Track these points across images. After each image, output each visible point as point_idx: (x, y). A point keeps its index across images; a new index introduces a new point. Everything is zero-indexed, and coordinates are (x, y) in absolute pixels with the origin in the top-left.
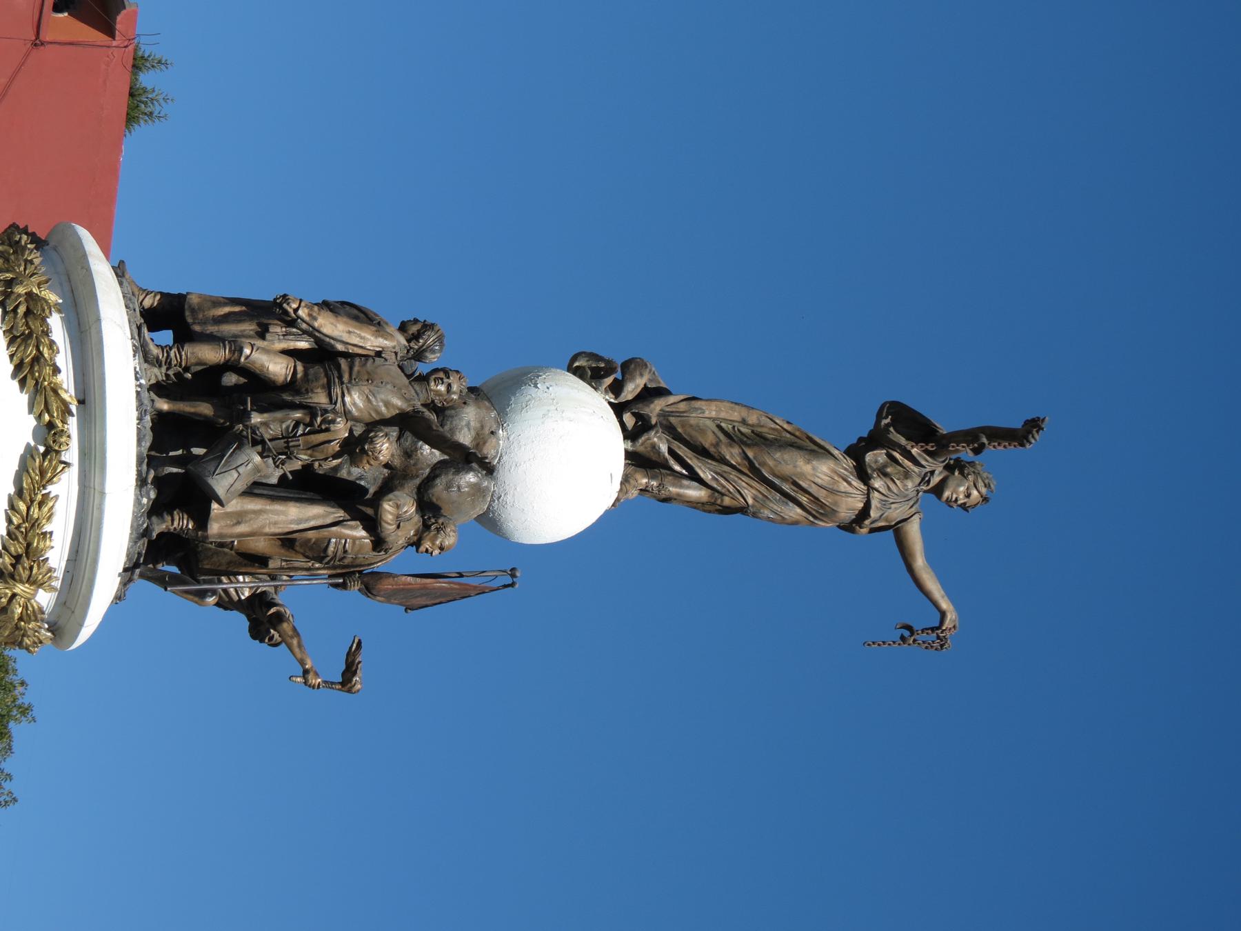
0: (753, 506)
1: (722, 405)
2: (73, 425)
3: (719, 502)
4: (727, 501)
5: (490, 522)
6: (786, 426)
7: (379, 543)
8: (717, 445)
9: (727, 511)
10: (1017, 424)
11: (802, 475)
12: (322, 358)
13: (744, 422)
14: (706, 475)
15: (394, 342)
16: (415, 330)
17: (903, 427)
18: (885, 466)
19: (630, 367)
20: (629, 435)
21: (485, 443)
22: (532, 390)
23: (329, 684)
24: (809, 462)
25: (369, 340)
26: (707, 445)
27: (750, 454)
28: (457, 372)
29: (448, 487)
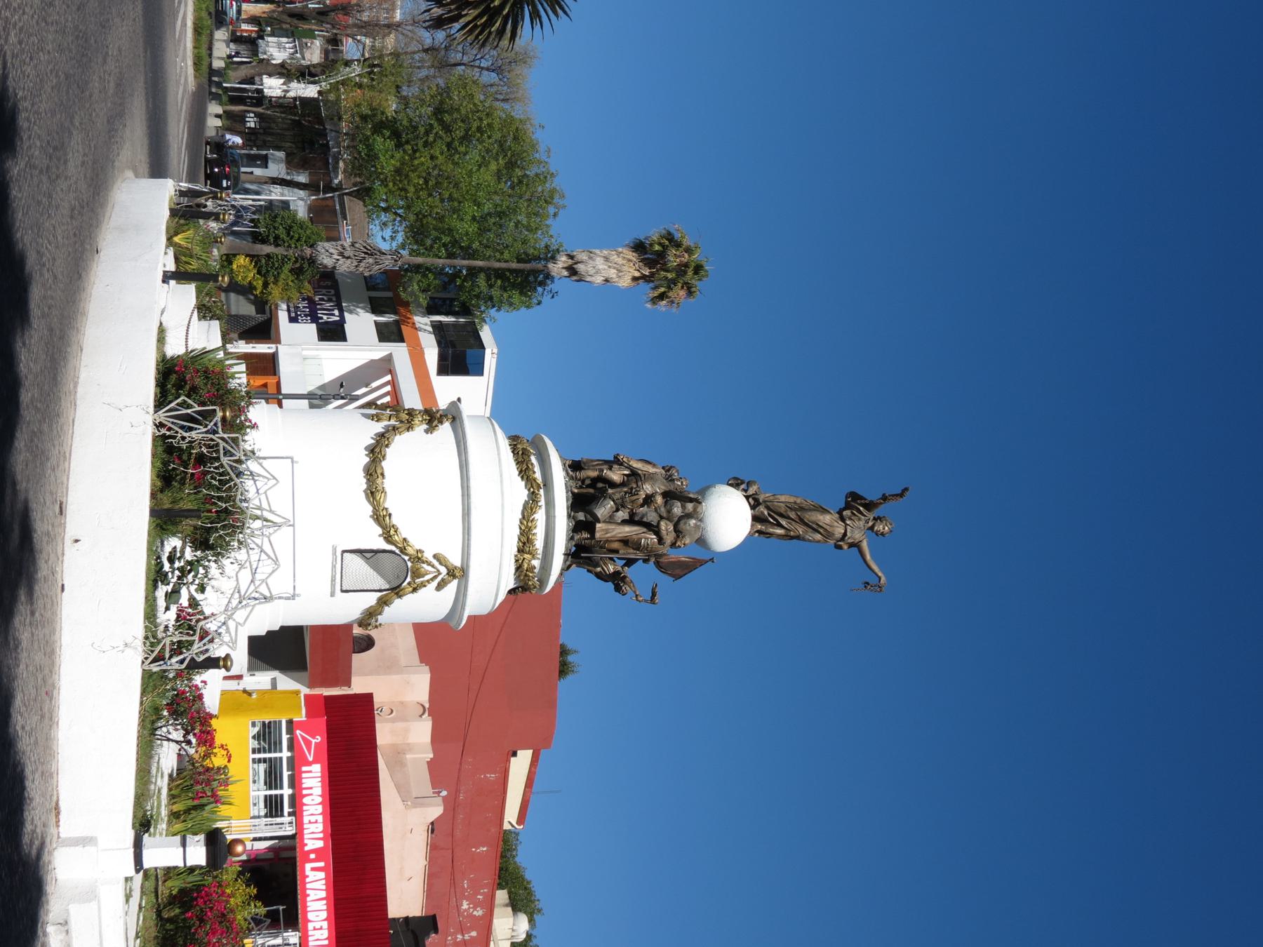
2: (542, 492)
5: (702, 542)
7: (661, 541)
9: (792, 538)
12: (634, 474)
14: (783, 522)
15: (660, 471)
16: (667, 469)
19: (749, 484)
20: (753, 507)
23: (646, 601)
25: (651, 470)
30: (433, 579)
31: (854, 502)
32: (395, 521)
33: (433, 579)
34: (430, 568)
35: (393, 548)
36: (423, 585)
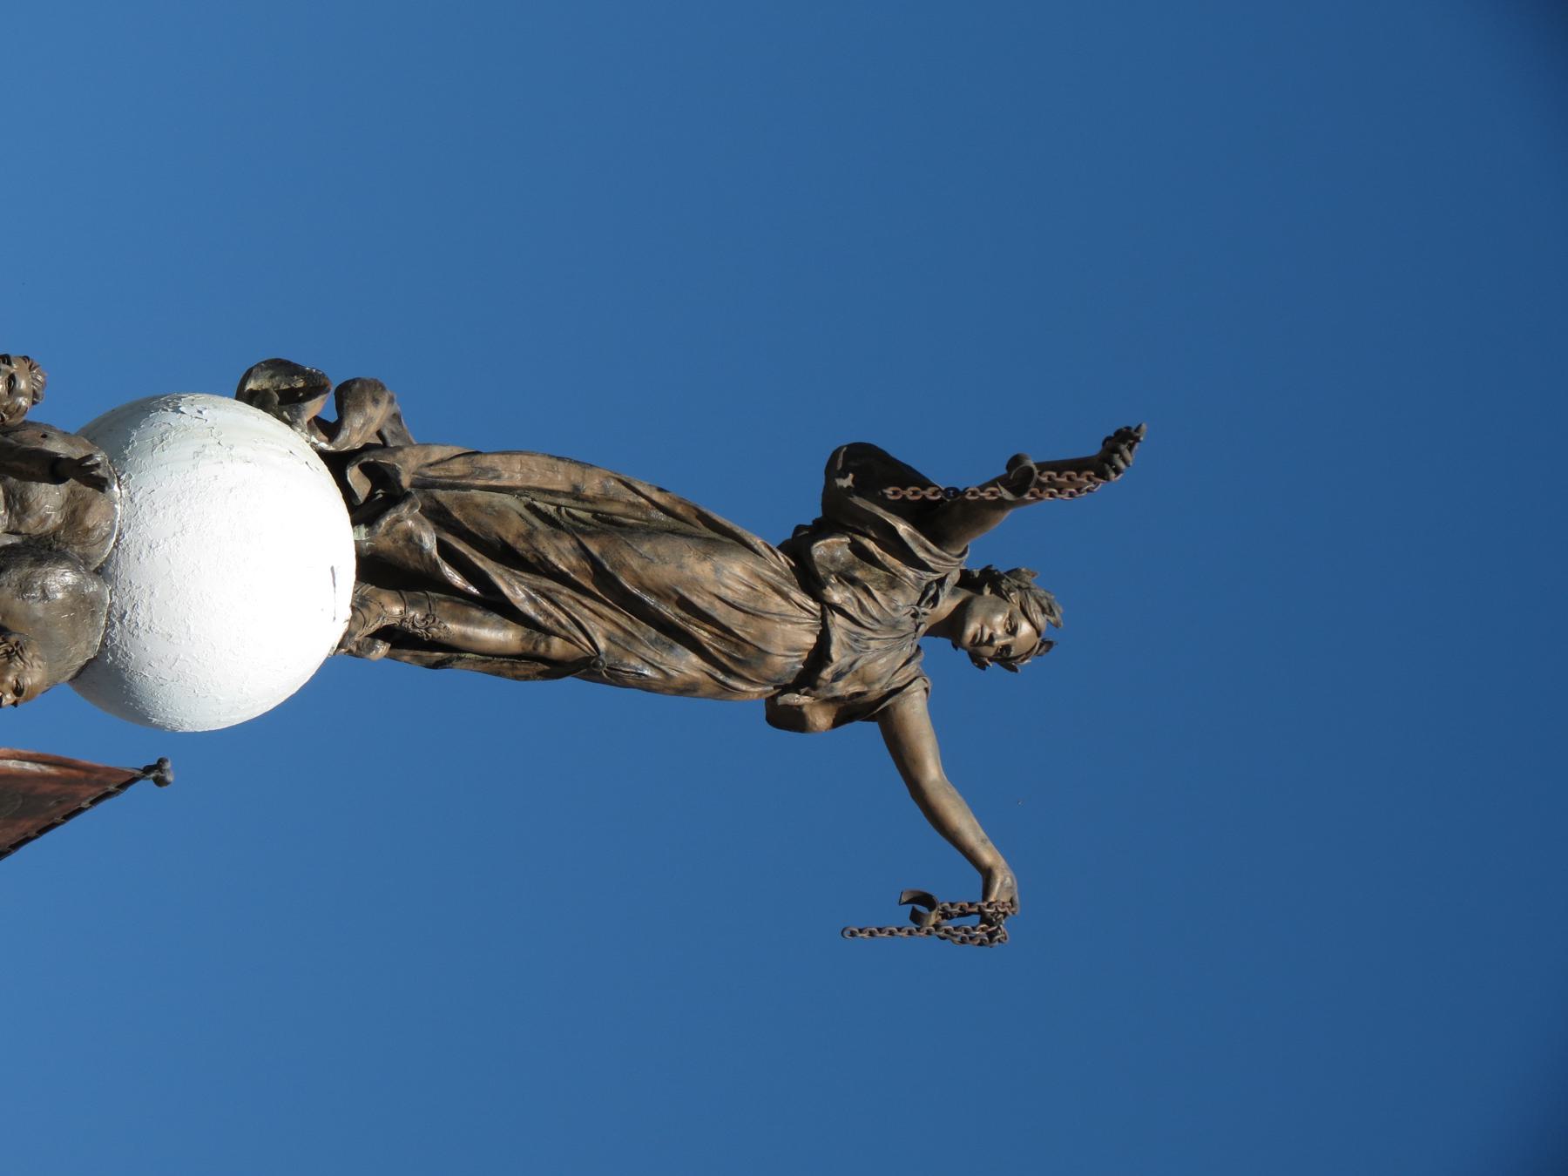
0: (608, 653)
1: (532, 462)
3: (542, 648)
4: (557, 647)
5: (106, 679)
6: (656, 496)
8: (529, 536)
9: (557, 668)
10: (1093, 449)
11: (694, 582)
13: (576, 494)
14: (516, 590)
17: (871, 499)
18: (852, 567)
19: (347, 396)
20: (362, 513)
21: (87, 507)
22: (171, 417)
24: (706, 557)
26: (510, 539)
27: (594, 549)
28: (26, 358)
29: (24, 588)
31: (871, 499)
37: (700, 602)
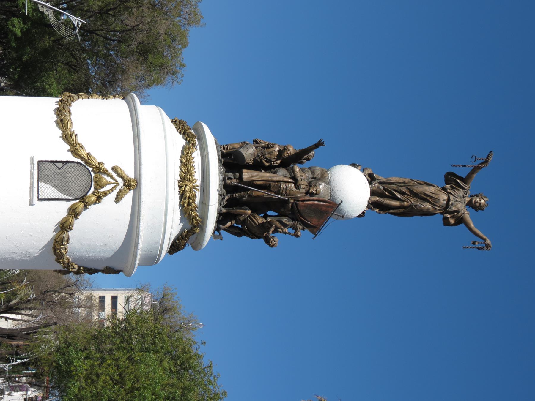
7: (297, 187)
14: (398, 196)
17: (452, 180)
20: (370, 183)
30: (112, 190)
31: (452, 180)
32: (80, 140)
33: (112, 190)
34: (109, 179)
35: (79, 161)
36: (106, 194)
37: (428, 193)
